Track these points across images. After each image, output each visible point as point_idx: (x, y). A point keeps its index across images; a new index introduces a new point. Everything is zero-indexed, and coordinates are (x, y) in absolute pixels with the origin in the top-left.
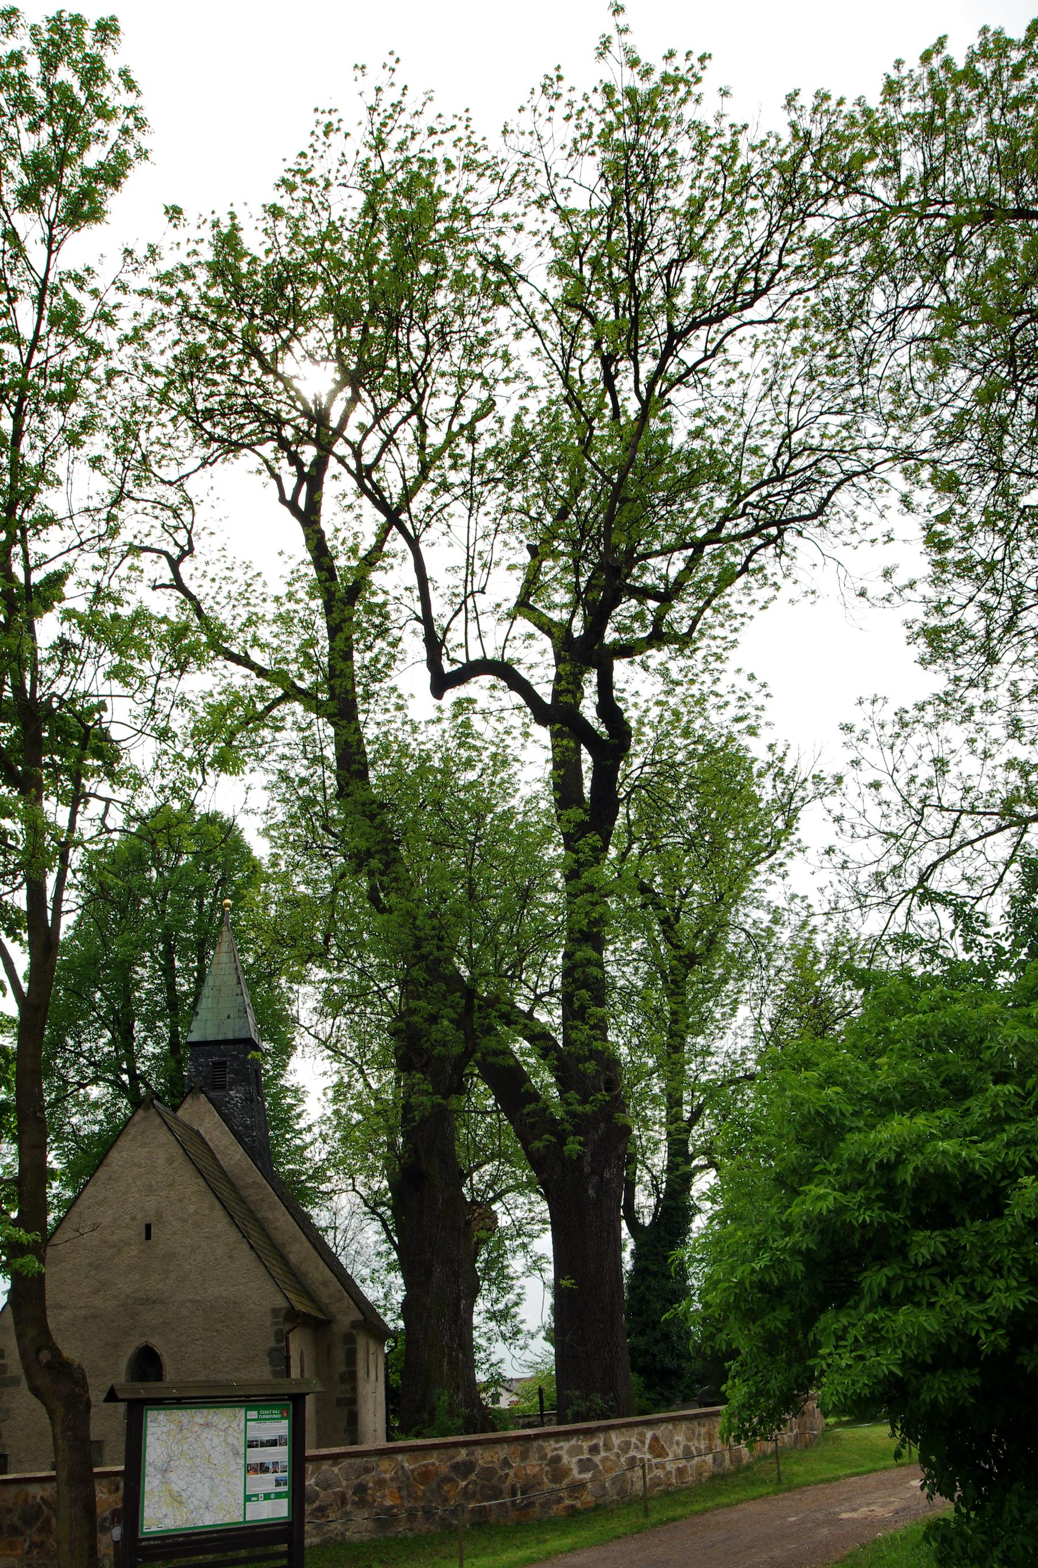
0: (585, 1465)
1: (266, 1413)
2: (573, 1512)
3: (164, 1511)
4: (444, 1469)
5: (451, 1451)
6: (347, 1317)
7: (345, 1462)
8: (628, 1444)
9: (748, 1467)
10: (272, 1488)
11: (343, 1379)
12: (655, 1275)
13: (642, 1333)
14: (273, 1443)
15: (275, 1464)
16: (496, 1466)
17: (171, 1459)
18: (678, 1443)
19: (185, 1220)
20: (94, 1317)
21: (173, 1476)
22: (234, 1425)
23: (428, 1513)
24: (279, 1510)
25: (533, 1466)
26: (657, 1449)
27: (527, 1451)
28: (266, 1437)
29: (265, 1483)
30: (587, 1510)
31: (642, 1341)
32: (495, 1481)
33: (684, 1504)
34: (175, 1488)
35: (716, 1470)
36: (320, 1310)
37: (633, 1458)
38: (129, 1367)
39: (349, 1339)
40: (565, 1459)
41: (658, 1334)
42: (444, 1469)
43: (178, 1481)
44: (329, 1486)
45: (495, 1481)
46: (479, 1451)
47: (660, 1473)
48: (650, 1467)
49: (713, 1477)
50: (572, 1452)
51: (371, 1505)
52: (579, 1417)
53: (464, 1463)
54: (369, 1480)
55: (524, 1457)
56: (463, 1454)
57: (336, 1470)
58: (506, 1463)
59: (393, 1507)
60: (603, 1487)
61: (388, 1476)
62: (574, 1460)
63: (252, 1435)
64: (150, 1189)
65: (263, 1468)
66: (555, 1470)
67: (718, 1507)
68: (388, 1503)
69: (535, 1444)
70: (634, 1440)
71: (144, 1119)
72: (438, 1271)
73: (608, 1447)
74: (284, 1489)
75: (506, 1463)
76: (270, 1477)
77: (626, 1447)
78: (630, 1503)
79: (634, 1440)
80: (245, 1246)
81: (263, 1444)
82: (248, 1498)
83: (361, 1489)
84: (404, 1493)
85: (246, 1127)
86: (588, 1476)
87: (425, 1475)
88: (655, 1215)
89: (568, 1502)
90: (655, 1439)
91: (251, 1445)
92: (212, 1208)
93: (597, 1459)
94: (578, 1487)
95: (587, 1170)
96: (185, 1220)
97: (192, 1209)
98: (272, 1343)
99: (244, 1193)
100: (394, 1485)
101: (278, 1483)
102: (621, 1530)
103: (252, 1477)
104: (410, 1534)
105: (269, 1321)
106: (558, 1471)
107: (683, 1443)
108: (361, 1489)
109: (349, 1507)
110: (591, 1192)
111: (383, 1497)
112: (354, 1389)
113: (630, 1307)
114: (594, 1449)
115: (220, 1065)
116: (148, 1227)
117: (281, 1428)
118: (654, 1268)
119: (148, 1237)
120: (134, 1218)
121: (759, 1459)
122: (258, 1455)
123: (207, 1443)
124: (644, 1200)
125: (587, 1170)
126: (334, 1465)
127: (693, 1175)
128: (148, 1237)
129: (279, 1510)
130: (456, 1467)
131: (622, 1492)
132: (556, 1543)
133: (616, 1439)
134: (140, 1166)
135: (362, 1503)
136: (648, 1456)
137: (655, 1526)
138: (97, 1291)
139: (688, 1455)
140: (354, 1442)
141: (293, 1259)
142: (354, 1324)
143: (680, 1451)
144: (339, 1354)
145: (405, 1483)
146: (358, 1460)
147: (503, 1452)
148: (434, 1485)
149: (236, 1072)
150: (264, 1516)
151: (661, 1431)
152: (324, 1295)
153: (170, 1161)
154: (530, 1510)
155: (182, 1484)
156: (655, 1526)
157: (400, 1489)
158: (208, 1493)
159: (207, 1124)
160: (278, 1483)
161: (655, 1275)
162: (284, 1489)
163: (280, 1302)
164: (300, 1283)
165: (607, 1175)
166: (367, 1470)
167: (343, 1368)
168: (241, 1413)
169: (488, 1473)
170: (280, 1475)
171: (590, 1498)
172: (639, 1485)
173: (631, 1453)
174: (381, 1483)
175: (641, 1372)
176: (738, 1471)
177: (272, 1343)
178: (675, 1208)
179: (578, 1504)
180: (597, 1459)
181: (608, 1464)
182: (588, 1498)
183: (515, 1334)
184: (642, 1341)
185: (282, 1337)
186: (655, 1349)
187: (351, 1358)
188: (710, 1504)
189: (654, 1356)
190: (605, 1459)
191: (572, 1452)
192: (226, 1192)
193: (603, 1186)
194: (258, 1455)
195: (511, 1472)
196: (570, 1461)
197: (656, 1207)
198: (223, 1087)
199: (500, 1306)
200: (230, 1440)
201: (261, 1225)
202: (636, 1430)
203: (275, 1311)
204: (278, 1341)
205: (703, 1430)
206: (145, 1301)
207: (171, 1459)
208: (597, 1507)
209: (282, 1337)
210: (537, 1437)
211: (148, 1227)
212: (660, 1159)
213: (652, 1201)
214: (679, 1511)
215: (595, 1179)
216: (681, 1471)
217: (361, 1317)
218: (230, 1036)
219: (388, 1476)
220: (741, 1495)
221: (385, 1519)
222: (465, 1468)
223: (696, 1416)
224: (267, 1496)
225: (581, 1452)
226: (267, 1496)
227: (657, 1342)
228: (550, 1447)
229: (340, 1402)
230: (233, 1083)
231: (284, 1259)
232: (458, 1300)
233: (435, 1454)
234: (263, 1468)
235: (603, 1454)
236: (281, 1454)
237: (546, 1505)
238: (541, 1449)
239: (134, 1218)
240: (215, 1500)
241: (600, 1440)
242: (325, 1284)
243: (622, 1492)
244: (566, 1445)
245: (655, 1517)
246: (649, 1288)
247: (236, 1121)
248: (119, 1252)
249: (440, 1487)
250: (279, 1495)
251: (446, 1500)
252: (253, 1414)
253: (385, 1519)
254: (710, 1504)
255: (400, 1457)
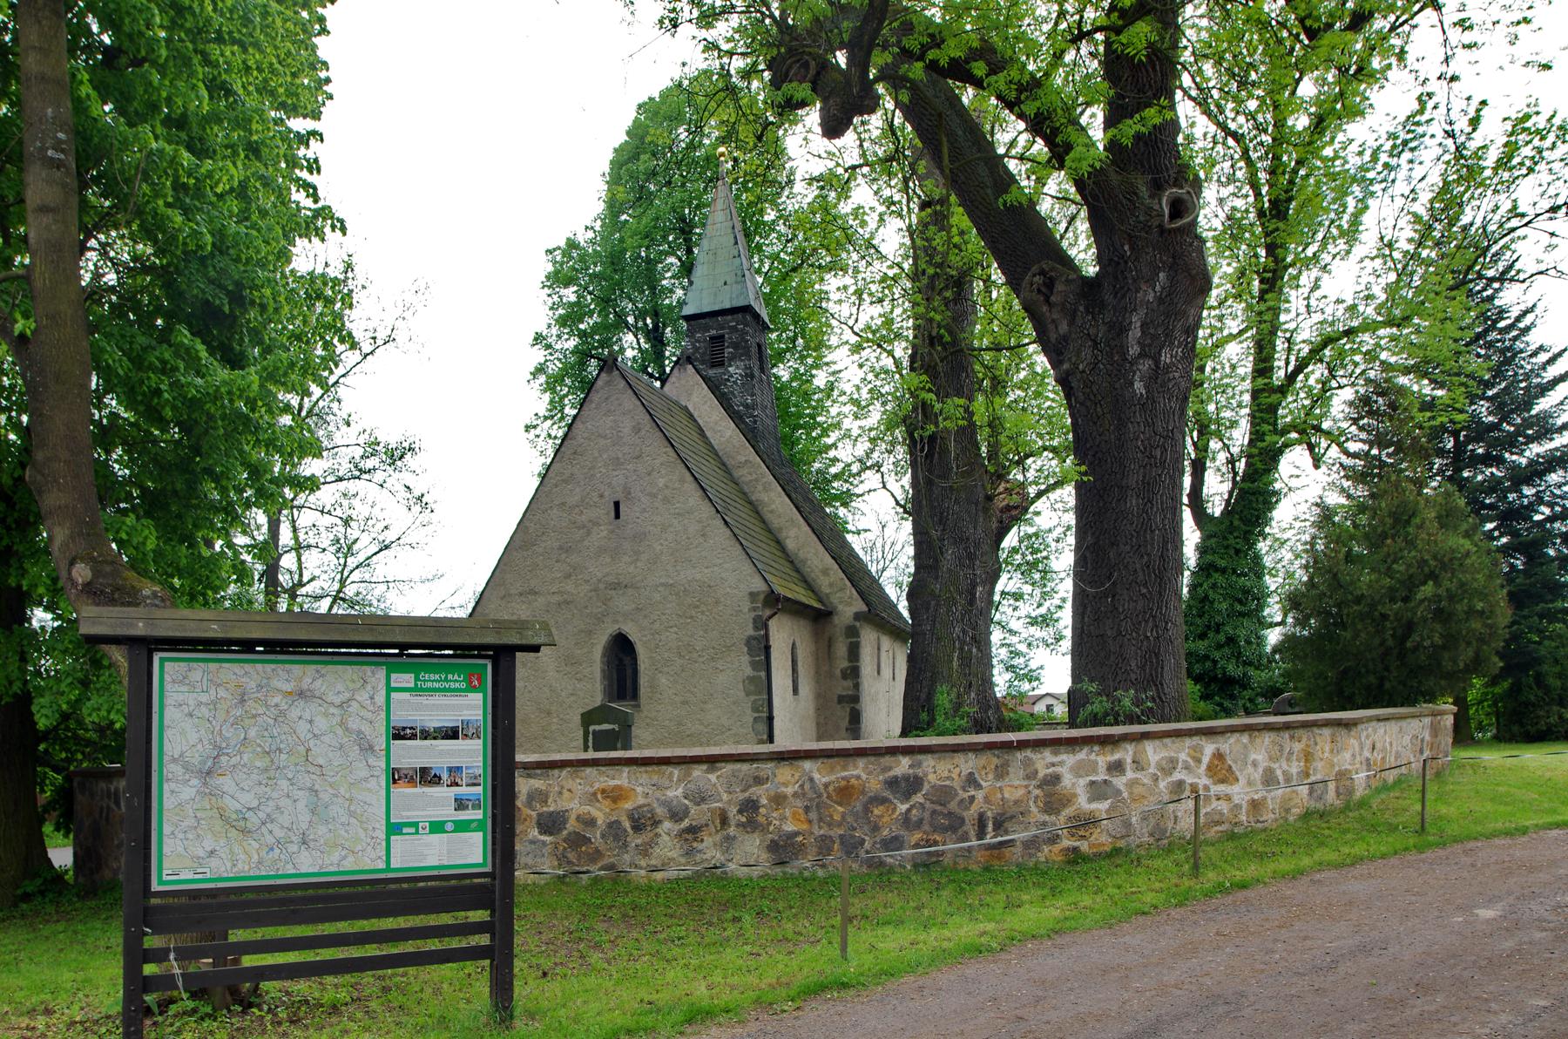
0: (1098, 791)
1: (431, 679)
2: (1075, 858)
3: (209, 844)
4: (875, 784)
5: (887, 760)
6: (848, 605)
7: (728, 768)
8: (1173, 763)
9: (1362, 804)
10: (448, 813)
11: (845, 676)
12: (1223, 571)
13: (1202, 636)
14: (452, 734)
15: (454, 770)
16: (956, 784)
17: (220, 752)
18: (1255, 764)
19: (655, 496)
20: (567, 603)
21: (226, 783)
22: (363, 696)
23: (851, 846)
24: (470, 851)
25: (1014, 787)
26: (1221, 770)
27: (1006, 765)
28: (432, 723)
29: (438, 802)
30: (1098, 856)
31: (1201, 646)
32: (953, 806)
33: (1261, 856)
34: (231, 804)
35: (1312, 804)
36: (820, 601)
37: (1180, 783)
38: (604, 655)
39: (852, 632)
40: (1067, 780)
41: (1222, 638)
42: (875, 784)
43: (238, 792)
44: (703, 800)
45: (953, 806)
46: (928, 762)
47: (1223, 806)
48: (1207, 798)
49: (1307, 815)
50: (1078, 770)
51: (763, 829)
52: (1096, 721)
53: (906, 778)
54: (762, 794)
55: (1001, 772)
56: (903, 766)
57: (713, 777)
58: (971, 781)
59: (797, 834)
60: (1127, 824)
61: (789, 790)
62: (1082, 782)
63: (401, 717)
64: (617, 463)
65: (426, 777)
66: (1048, 795)
67: (1321, 866)
68: (789, 827)
69: (1019, 755)
70: (1183, 756)
71: (608, 383)
72: (950, 553)
73: (1138, 765)
74: (477, 815)
75: (971, 781)
76: (444, 793)
77: (1170, 766)
78: (1169, 850)
79: (1183, 756)
80: (719, 523)
81: (426, 735)
82: (395, 829)
83: (750, 806)
84: (813, 815)
85: (747, 406)
86: (1102, 807)
87: (845, 792)
88: (1228, 502)
89: (1067, 843)
90: (1219, 756)
91: (399, 734)
92: (682, 481)
93: (1120, 782)
94: (1085, 823)
95: (1134, 350)
96: (655, 496)
97: (661, 482)
98: (751, 632)
99: (736, 474)
100: (799, 803)
101: (460, 804)
102: (1149, 898)
103: (403, 791)
104: (820, 873)
105: (746, 605)
106: (1054, 799)
107: (1263, 764)
108: (750, 806)
109: (732, 831)
110: (1139, 386)
111: (783, 818)
112: (857, 686)
113: (1189, 607)
114: (1117, 767)
115: (718, 339)
116: (617, 504)
117: (473, 707)
118: (1223, 563)
119: (617, 516)
120: (601, 496)
121: (1378, 791)
122: (412, 754)
123: (303, 728)
124: (1217, 489)
125: (1134, 350)
126: (711, 770)
127: (1281, 452)
128: (617, 516)
129: (470, 851)
130: (893, 783)
131: (1158, 833)
132: (1035, 913)
133: (1154, 753)
134: (605, 437)
135: (751, 825)
136: (1203, 781)
137: (1208, 895)
138: (568, 576)
139: (1269, 779)
140: (857, 738)
141: (790, 545)
142: (857, 616)
143: (1257, 776)
144: (841, 649)
145: (814, 803)
146: (745, 767)
147: (967, 764)
148: (859, 807)
149: (735, 346)
150: (432, 861)
151: (1229, 744)
152: (824, 584)
153: (637, 429)
154: (1007, 851)
155: (249, 799)
156: (1208, 895)
157: (807, 809)
158: (305, 818)
159: (695, 398)
160: (460, 804)
161: (1223, 571)
162: (477, 815)
163: (758, 585)
164: (797, 571)
165: (1166, 358)
166: (759, 781)
167: (845, 664)
168: (377, 676)
169: (943, 794)
170: (463, 790)
171: (1104, 838)
172: (1186, 824)
173: (1177, 776)
174: (778, 800)
175: (1197, 679)
176: (1347, 808)
177: (751, 632)
178: (1254, 498)
179: (1084, 846)
180: (1120, 782)
181: (1138, 790)
182: (1101, 838)
183: (1058, 640)
184: (1201, 646)
185: (762, 624)
186: (1217, 655)
187: (854, 652)
188: (1306, 861)
189: (1215, 662)
190: (1132, 783)
191: (1078, 770)
192: (707, 470)
193: (1158, 375)
194: (412, 754)
195: (980, 795)
196: (1069, 781)
197: (1231, 493)
198: (721, 364)
199: (1043, 610)
200: (354, 724)
201: (755, 509)
202: (1188, 742)
203: (753, 596)
204: (756, 628)
205: (1297, 747)
206: (615, 586)
207: (220, 752)
208: (1116, 851)
209: (762, 624)
210: (1022, 745)
211: (617, 504)
212: (1240, 436)
213: (1227, 486)
214: (1252, 870)
215: (1145, 365)
216: (1255, 805)
217: (865, 608)
218: (727, 305)
219: (789, 790)
220: (1359, 849)
221: (783, 849)
222: (908, 786)
223: (1287, 726)
224: (437, 827)
225: (1095, 771)
226: (437, 827)
227: (1219, 646)
228: (1044, 761)
229: (841, 699)
230: (732, 358)
231: (780, 544)
232: (974, 586)
233: (861, 762)
234: (426, 777)
235: (1130, 774)
236: (472, 754)
237: (1032, 844)
238: (1027, 763)
239: (601, 496)
240: (322, 830)
241: (1126, 753)
242: (825, 572)
243: (1158, 833)
244: (1069, 759)
245: (1211, 876)
246: (1214, 586)
247: (737, 400)
248: (589, 533)
249: (867, 810)
250: (462, 826)
251: (876, 828)
252: (405, 679)
253: (783, 849)
254: (1306, 861)
255: (807, 765)
